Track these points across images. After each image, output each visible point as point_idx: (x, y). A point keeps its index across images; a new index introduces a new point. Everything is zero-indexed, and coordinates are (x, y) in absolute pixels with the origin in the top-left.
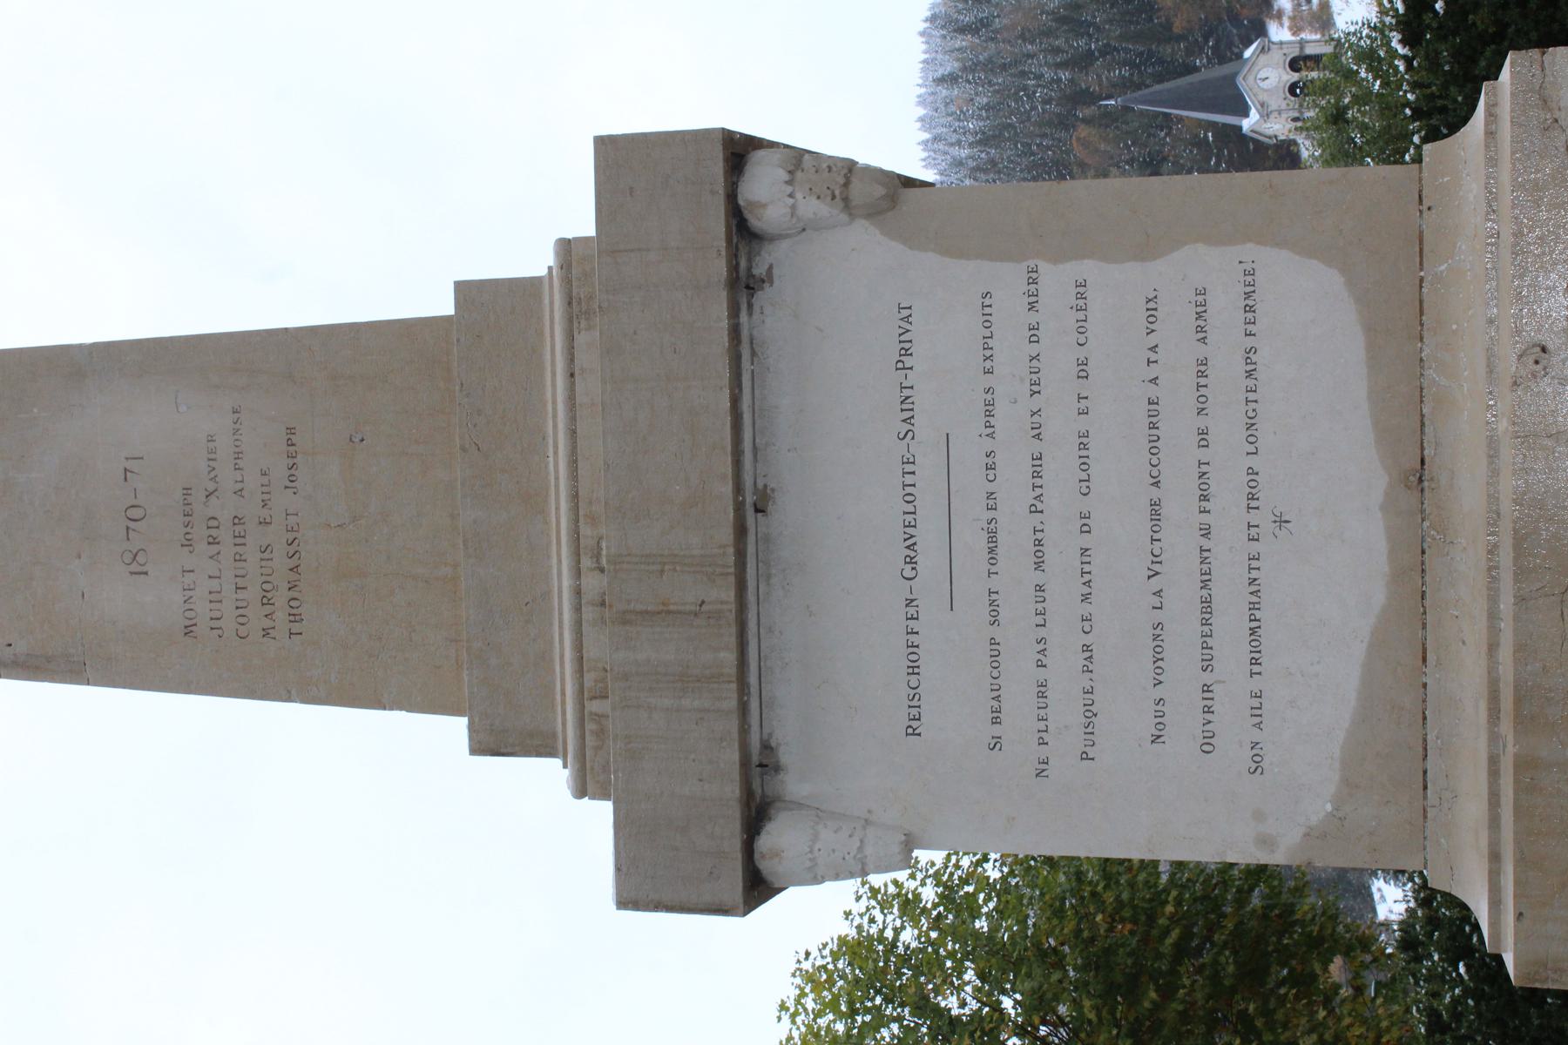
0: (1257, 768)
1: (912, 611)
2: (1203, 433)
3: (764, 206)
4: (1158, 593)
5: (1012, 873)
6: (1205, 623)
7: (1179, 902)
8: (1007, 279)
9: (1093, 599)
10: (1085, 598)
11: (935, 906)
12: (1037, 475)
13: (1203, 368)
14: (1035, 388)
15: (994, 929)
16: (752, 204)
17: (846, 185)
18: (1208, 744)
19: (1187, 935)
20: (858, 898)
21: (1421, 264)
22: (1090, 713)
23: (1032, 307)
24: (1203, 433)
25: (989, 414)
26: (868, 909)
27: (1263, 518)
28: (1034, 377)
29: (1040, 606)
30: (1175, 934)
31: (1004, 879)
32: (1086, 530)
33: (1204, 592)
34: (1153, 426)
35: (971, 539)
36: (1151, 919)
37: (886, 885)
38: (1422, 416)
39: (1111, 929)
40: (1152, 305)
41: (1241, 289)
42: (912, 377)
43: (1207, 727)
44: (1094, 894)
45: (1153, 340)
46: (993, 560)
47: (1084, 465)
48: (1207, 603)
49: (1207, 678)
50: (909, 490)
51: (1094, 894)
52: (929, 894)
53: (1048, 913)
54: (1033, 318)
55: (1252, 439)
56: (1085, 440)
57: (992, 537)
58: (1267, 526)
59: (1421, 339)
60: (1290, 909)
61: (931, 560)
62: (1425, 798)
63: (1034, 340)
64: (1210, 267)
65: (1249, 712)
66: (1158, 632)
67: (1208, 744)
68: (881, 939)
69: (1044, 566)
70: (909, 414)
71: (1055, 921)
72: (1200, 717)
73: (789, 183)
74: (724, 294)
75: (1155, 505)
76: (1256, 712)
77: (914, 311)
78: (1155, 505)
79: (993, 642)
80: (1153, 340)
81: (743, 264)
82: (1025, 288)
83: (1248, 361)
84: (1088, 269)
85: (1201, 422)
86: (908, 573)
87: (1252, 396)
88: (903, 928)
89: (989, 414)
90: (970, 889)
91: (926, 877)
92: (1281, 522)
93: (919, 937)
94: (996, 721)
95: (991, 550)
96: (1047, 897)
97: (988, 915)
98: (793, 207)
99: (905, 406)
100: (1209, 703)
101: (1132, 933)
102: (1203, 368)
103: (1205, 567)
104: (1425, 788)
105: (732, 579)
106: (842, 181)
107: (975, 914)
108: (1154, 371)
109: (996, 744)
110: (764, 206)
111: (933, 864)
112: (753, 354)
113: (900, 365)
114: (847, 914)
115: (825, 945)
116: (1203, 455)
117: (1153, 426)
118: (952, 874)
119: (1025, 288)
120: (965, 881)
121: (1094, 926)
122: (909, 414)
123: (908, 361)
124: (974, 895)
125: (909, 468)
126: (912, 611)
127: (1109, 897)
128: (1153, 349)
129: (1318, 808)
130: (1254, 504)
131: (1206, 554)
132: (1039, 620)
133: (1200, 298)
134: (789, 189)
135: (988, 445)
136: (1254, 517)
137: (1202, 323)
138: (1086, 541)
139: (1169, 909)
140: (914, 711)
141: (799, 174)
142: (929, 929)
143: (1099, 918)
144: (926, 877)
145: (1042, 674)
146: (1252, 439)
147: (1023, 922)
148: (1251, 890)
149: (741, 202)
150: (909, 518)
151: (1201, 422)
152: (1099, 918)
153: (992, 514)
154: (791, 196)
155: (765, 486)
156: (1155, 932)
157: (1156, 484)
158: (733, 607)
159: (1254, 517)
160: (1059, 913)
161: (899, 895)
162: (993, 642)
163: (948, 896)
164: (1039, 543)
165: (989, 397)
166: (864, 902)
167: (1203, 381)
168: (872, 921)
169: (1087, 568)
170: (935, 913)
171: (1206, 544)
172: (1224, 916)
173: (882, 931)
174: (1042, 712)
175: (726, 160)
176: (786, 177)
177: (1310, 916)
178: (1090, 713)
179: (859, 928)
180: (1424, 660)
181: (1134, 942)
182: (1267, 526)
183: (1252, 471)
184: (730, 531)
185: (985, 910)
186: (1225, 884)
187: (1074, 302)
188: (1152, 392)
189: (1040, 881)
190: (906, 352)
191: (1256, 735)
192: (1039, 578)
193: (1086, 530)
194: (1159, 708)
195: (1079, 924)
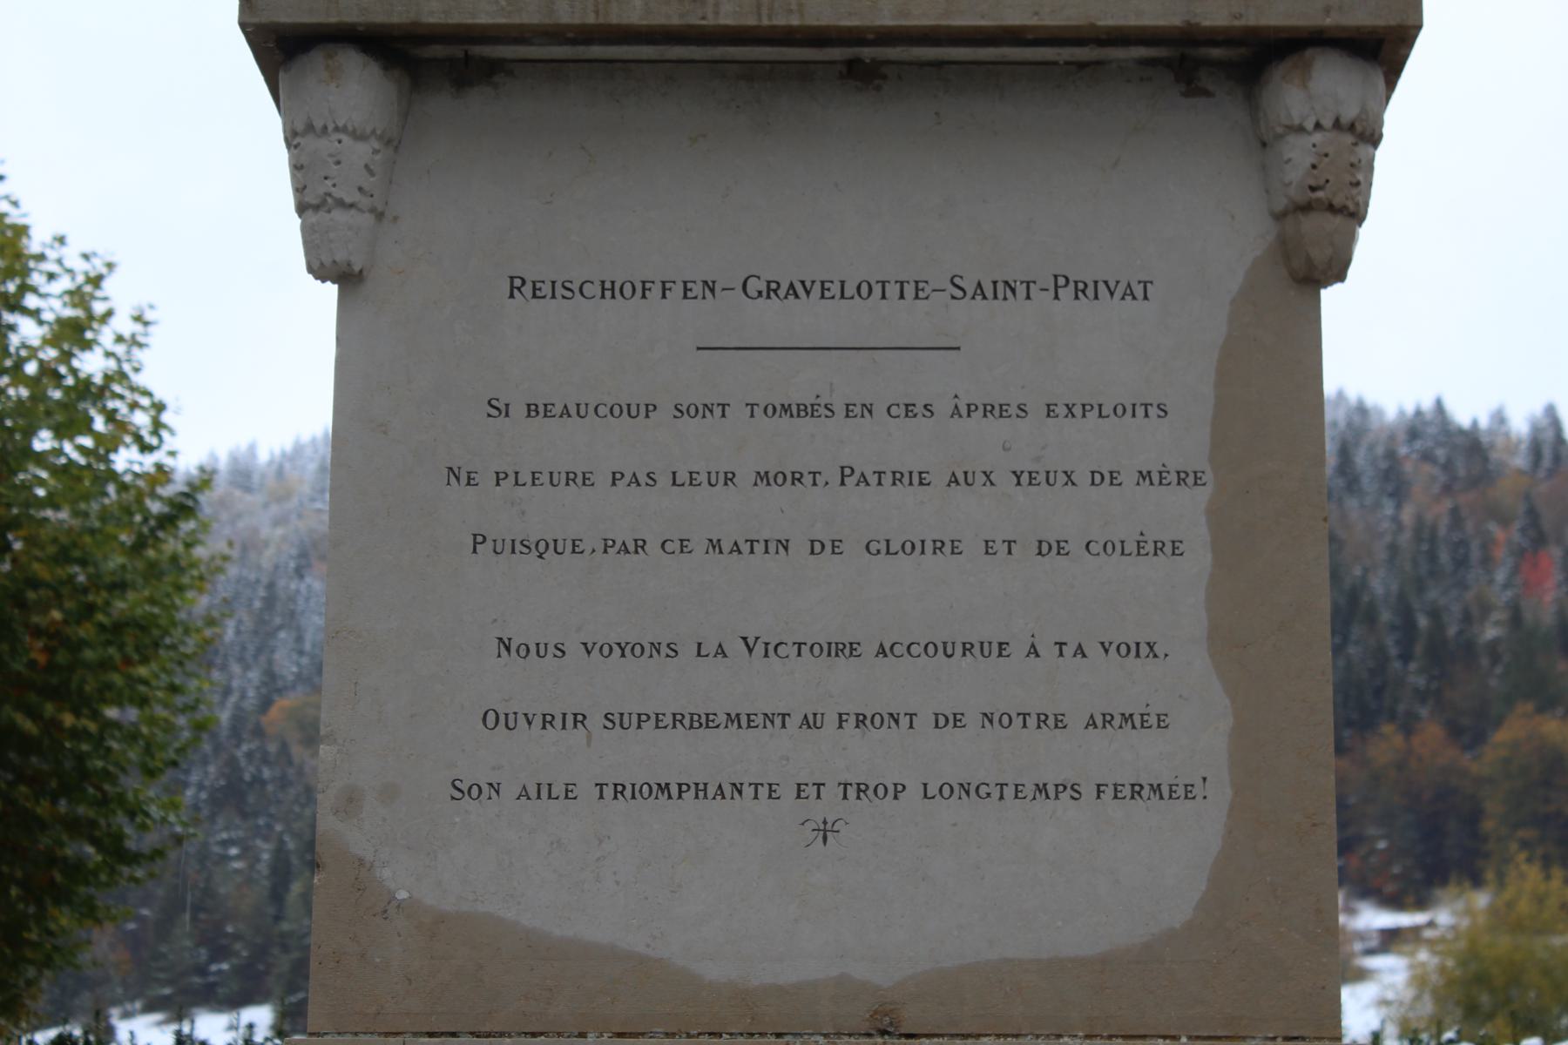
0: (460, 791)
1: (697, 289)
2: (956, 720)
3: (1304, 86)
4: (721, 651)
5: (123, 488)
6: (677, 719)
7: (77, 734)
8: (1184, 439)
9: (714, 555)
10: (715, 545)
11: (74, 372)
12: (897, 478)
13: (1051, 722)
14: (1025, 478)
15: (41, 459)
16: (1307, 67)
17: (1331, 208)
18: (497, 719)
19: (27, 745)
20: (86, 257)
21: (1198, 1038)
22: (544, 548)
23: (1144, 476)
24: (956, 720)
25: (988, 410)
26: (70, 271)
27: (829, 806)
28: (1041, 478)
29: (703, 478)
30: (28, 726)
31: (113, 476)
32: (815, 547)
33: (722, 718)
34: (967, 648)
35: (805, 379)
36: (58, 694)
37: (105, 299)
38: (978, 1036)
39: (37, 632)
40: (1144, 650)
41: (1165, 780)
42: (1042, 299)
43: (522, 721)
44: (91, 609)
45: (1094, 650)
46: (771, 410)
47: (908, 548)
48: (705, 721)
49: (596, 721)
50: (877, 289)
51: (91, 609)
52: (92, 364)
53: (64, 540)
54: (1128, 477)
55: (947, 790)
56: (947, 549)
57: (806, 410)
58: (819, 810)
59: (1088, 1037)
60: (63, 897)
61: (771, 318)
62: (415, 1034)
63: (1096, 478)
64: (1200, 738)
65: (545, 781)
66: (664, 650)
67: (497, 719)
68: (25, 288)
69: (762, 485)
70: (989, 293)
71: (52, 550)
72: (538, 709)
73: (1337, 124)
74: (1176, 21)
75: (850, 649)
76: (544, 791)
77: (1140, 302)
78: (850, 649)
79: (650, 408)
80: (1094, 650)
81: (1216, 53)
82: (1172, 467)
83: (1061, 787)
84: (1198, 560)
85: (972, 719)
86: (754, 286)
87: (1009, 792)
88: (41, 323)
89: (988, 410)
90: (99, 424)
91: (119, 360)
92: (825, 832)
93: (24, 346)
94: (532, 410)
95: (786, 409)
96: (88, 539)
97: (59, 452)
98: (1301, 129)
99: (1000, 286)
100: (558, 722)
101: (32, 664)
102: (1051, 722)
103: (759, 720)
104: (431, 1035)
105: (751, 21)
106: (1338, 201)
107: (60, 432)
108: (1048, 651)
109: (498, 409)
110: (1304, 86)
111: (137, 370)
112: (1082, 65)
113: (1061, 281)
114: (61, 240)
115: (15, 204)
116: (924, 720)
117: (967, 648)
118: (121, 397)
119: (1172, 467)
120: (111, 416)
121: (44, 608)
122: (989, 293)
123: (1067, 293)
124: (87, 428)
125: (909, 290)
126: (697, 289)
127: (85, 631)
128: (1080, 651)
129: (400, 878)
130: (852, 792)
131: (778, 721)
132: (683, 477)
133: (1153, 720)
134: (1327, 122)
135: (943, 407)
136: (832, 792)
137: (1116, 722)
138: (799, 547)
139: (68, 720)
140: (546, 289)
141: (1348, 139)
142: (41, 362)
143: (57, 615)
144: (119, 360)
145: (602, 479)
146: (947, 790)
147: (52, 502)
148: (95, 842)
149: (1309, 52)
150: (835, 289)
151: (972, 719)
152: (57, 615)
153: (840, 410)
154: (1318, 126)
155: (884, 77)
156: (32, 697)
157: (882, 651)
158: (711, 21)
159: (832, 792)
160: (64, 556)
161: (91, 317)
162: (650, 408)
163: (86, 390)
164: (797, 478)
165: (1013, 410)
166: (80, 266)
167: (1032, 722)
168: (51, 276)
169: (759, 548)
170: (63, 370)
171: (794, 721)
172: (54, 801)
173: (34, 290)
174: (545, 478)
175: (1374, 31)
176: (1345, 120)
177: (53, 926)
178: (544, 548)
179: (41, 257)
180: (620, 1035)
181: (18, 666)
182: (819, 810)
183: (899, 790)
184: (825, 21)
185: (68, 447)
186: (104, 802)
187: (1150, 538)
188: (1018, 649)
189: (110, 529)
190: (1080, 291)
191: (510, 790)
192: (745, 476)
193: (815, 547)
194: (551, 649)
195: (48, 586)
